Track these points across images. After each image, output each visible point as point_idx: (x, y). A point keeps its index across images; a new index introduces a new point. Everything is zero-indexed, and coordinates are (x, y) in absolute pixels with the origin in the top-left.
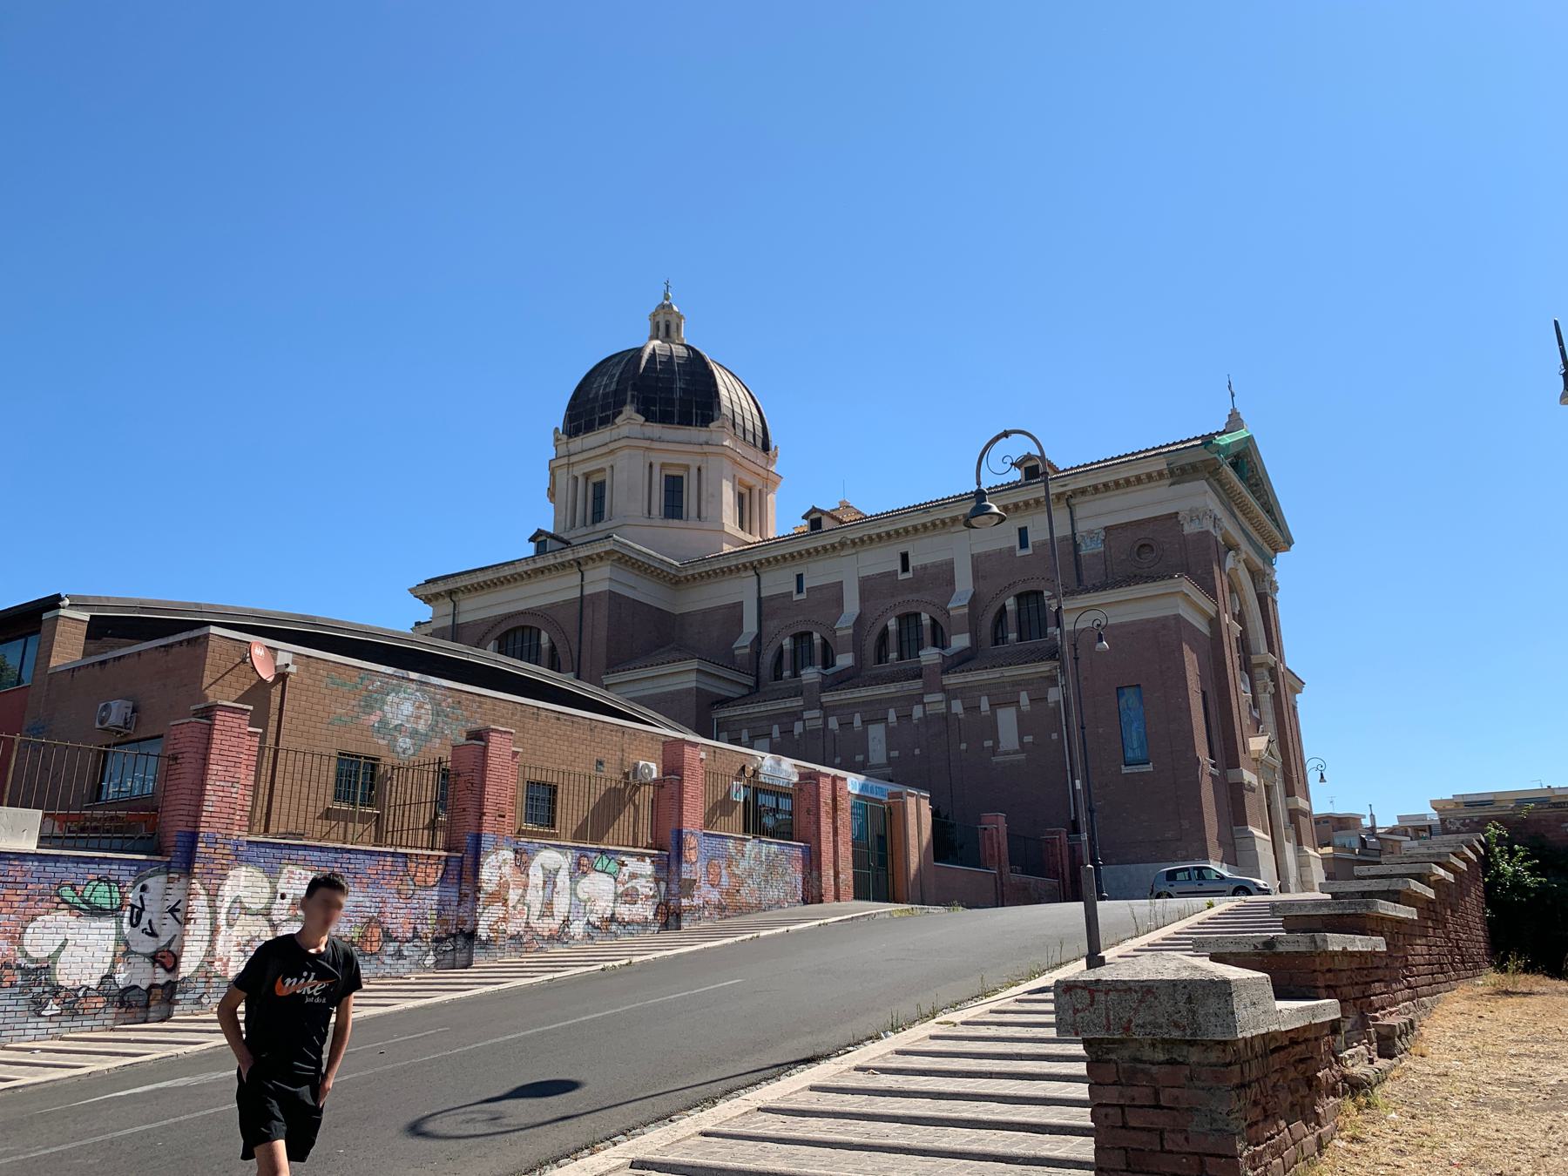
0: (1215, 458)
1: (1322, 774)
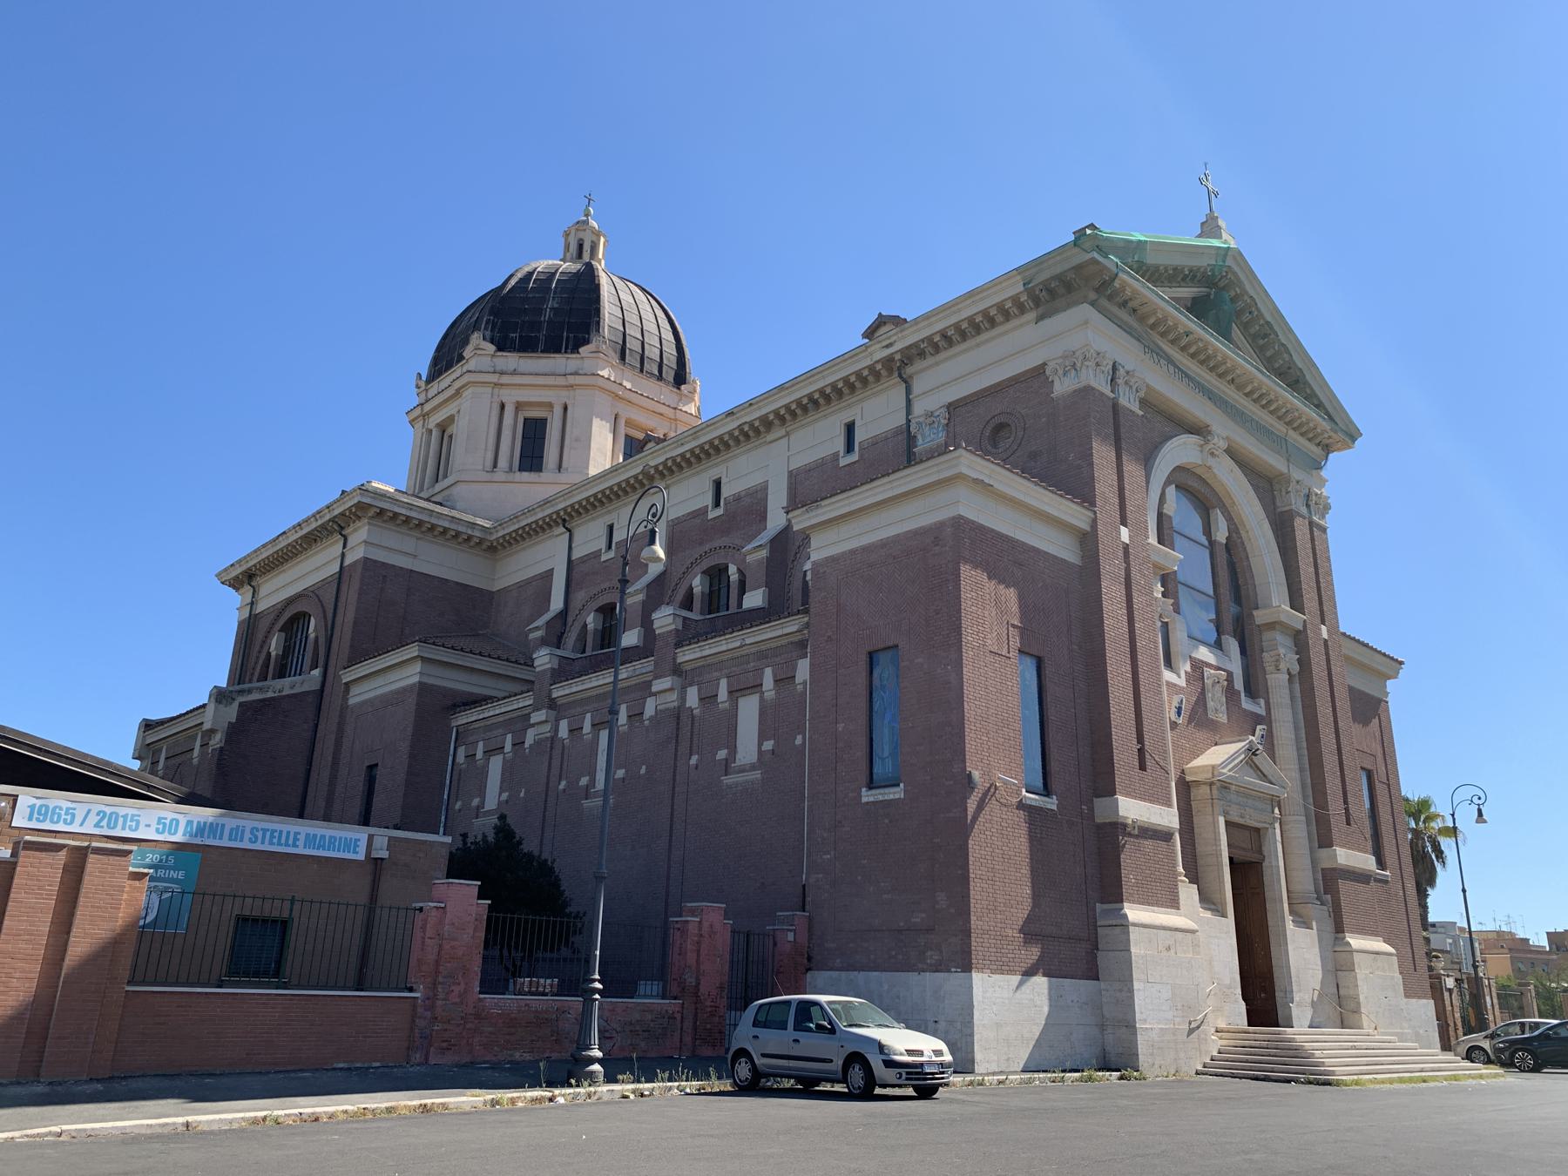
0: (1094, 261)
1: (1480, 811)
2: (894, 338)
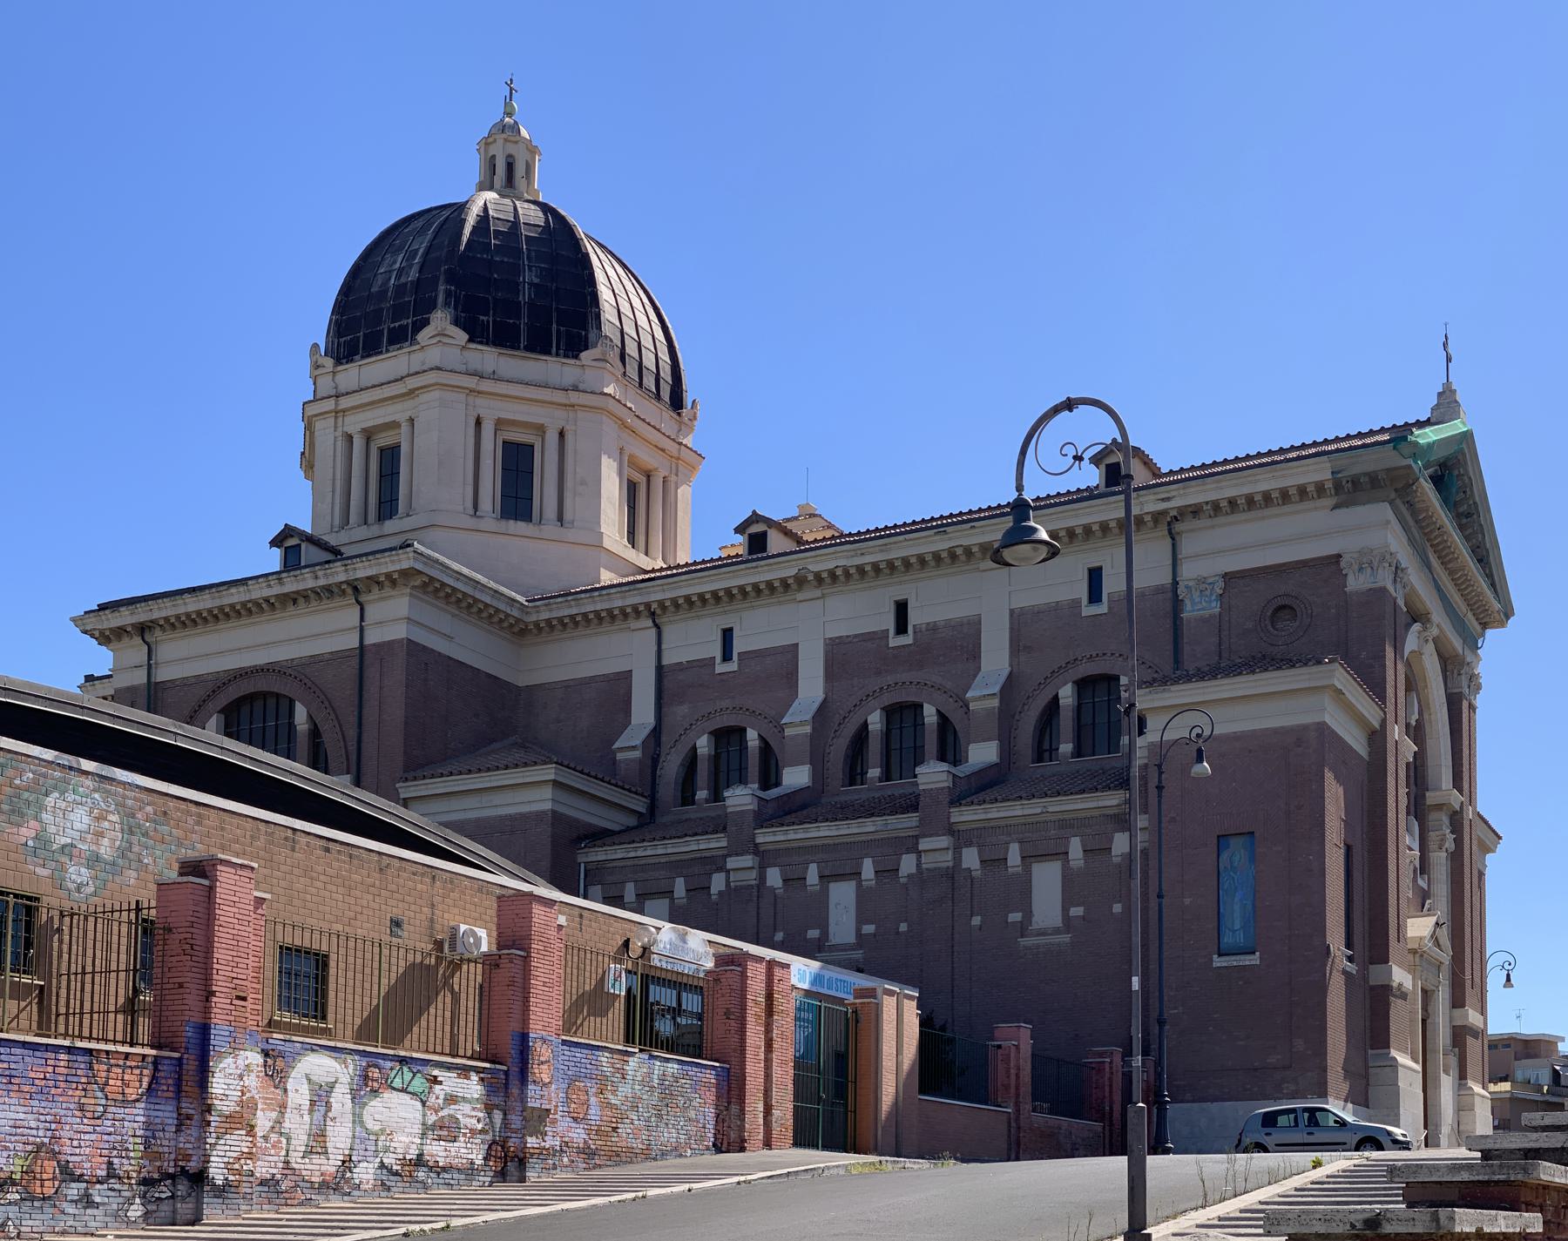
1: (1508, 975)
2: (1173, 494)
